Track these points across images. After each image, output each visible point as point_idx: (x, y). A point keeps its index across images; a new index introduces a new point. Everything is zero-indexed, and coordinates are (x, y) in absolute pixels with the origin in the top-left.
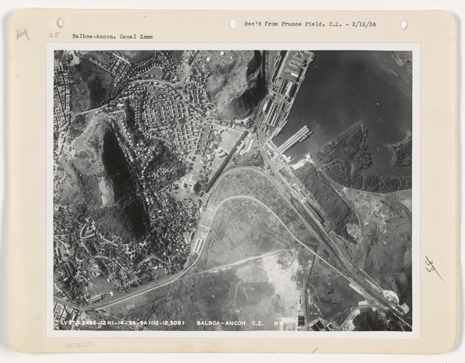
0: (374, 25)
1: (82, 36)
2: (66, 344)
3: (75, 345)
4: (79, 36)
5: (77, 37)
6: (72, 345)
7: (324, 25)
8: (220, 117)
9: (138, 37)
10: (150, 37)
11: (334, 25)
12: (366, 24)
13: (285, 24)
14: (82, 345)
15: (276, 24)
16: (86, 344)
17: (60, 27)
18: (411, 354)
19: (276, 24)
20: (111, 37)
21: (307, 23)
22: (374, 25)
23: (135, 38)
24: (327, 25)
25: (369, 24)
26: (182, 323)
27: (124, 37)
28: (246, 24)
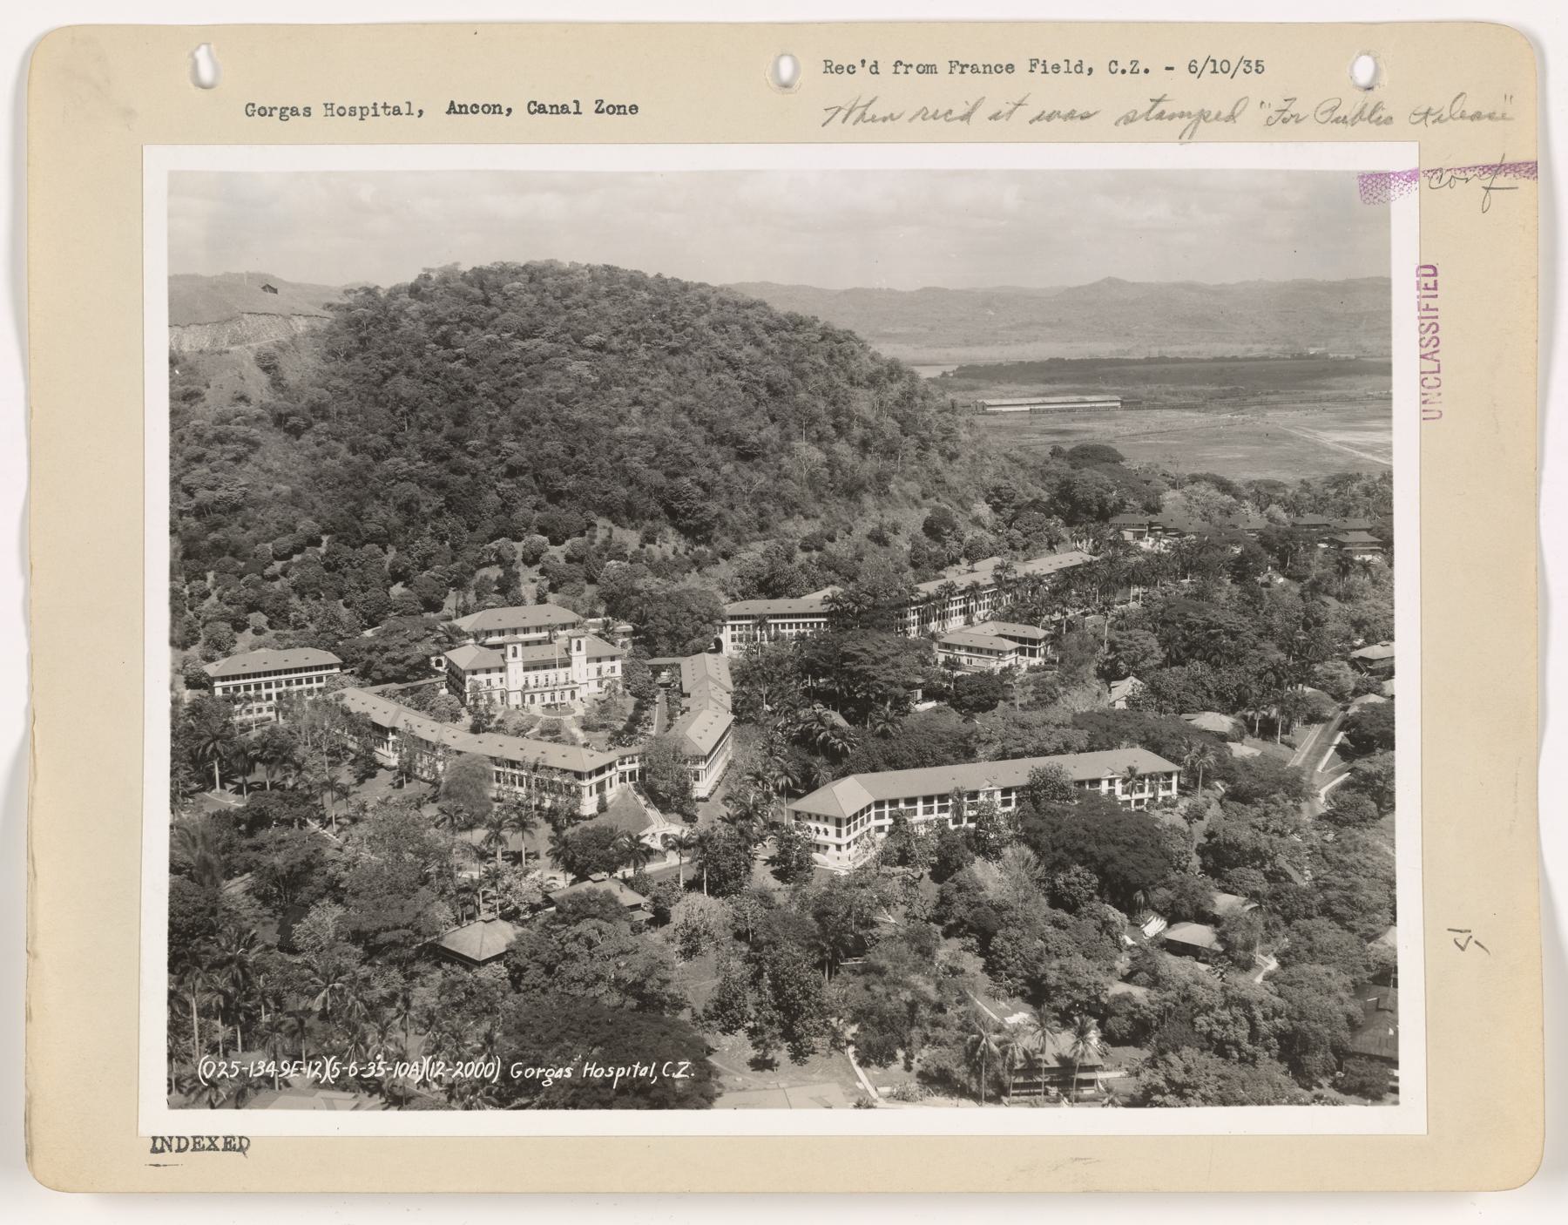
0: (1259, 67)
2: (154, 1139)
6: (175, 1141)
9: (588, 107)
10: (634, 109)
11: (1124, 72)
12: (1243, 66)
13: (959, 68)
14: (207, 1143)
15: (929, 69)
16: (220, 1143)
17: (204, 87)
19: (929, 69)
20: (495, 109)
21: (1034, 63)
22: (1259, 67)
23: (578, 113)
27: (542, 109)
28: (452, 109)
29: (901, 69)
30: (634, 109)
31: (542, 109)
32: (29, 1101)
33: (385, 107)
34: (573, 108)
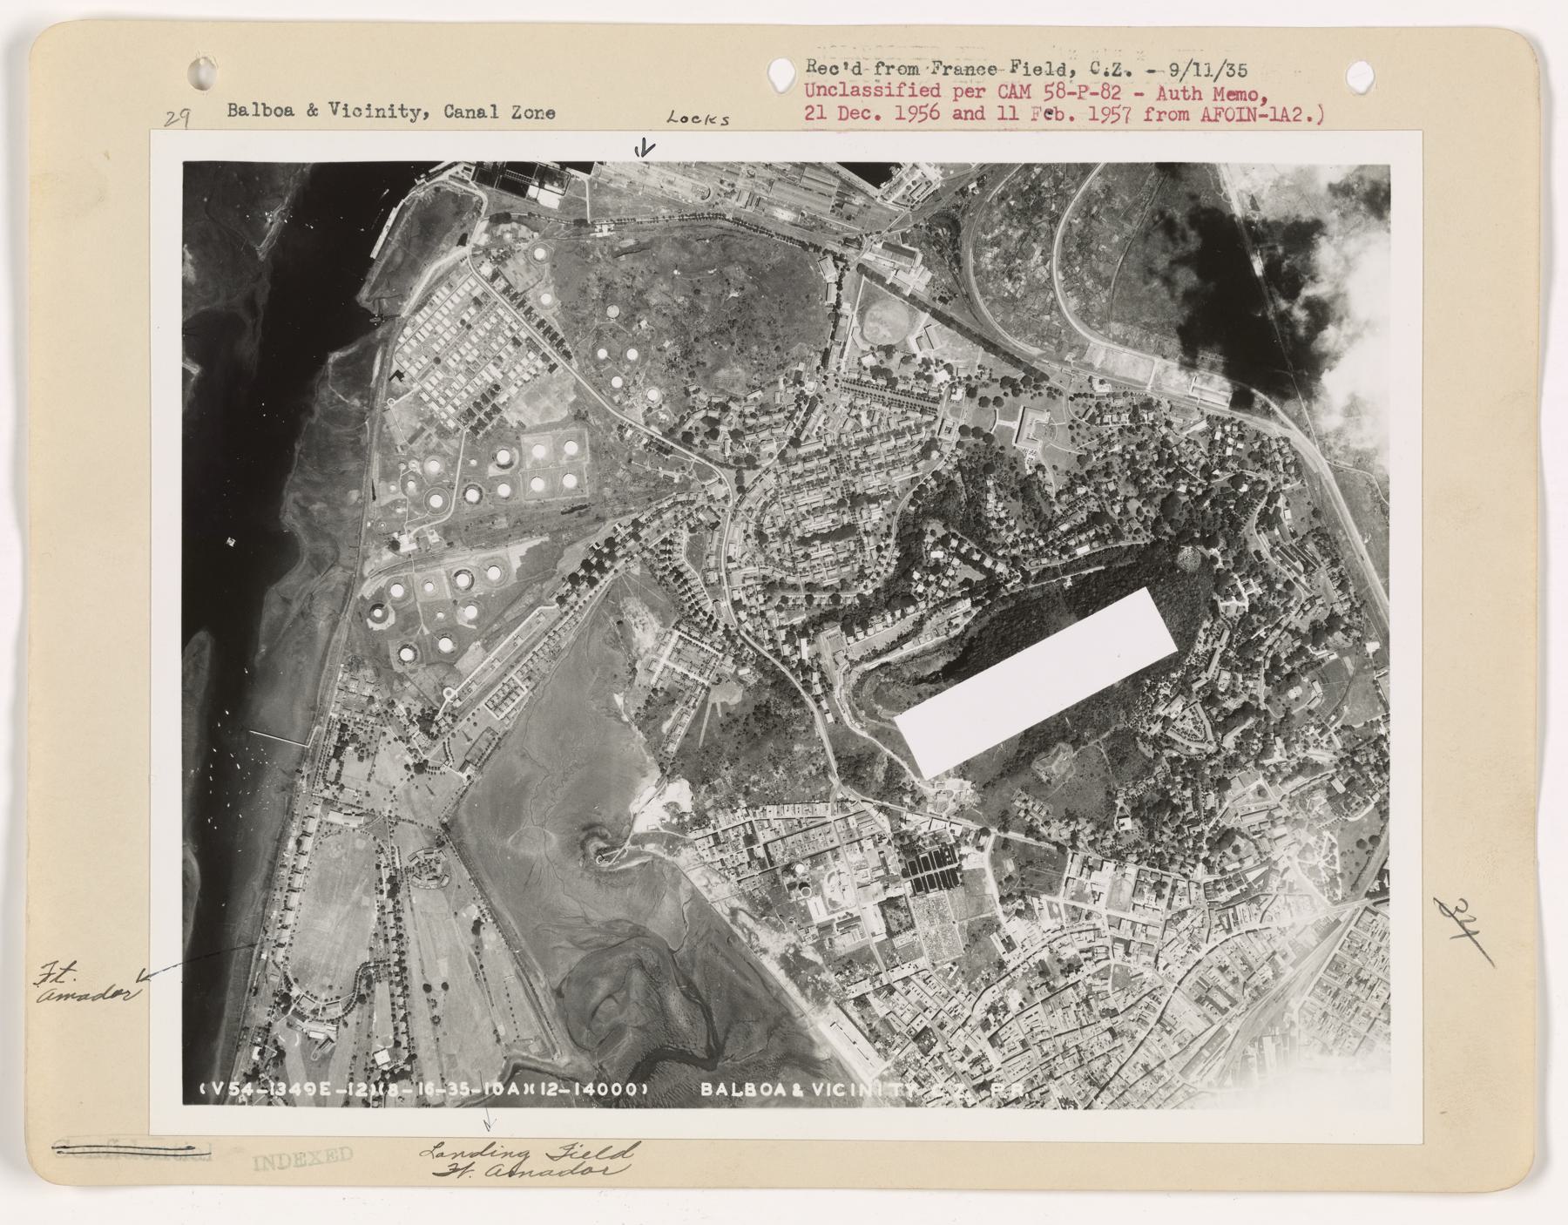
1: (261, 108)
3: (285, 1159)
4: (251, 110)
5: (243, 112)
6: (276, 1160)
7: (426, 114)
8: (1360, 843)
9: (505, 112)
12: (1214, 72)
13: (942, 69)
18: (264, 21)
24: (437, 113)
25: (1226, 69)
26: (640, 1090)
27: (458, 113)
29: (883, 70)
30: (551, 114)
31: (458, 113)
32: (27, 1109)
33: (402, 109)
34: (489, 112)
